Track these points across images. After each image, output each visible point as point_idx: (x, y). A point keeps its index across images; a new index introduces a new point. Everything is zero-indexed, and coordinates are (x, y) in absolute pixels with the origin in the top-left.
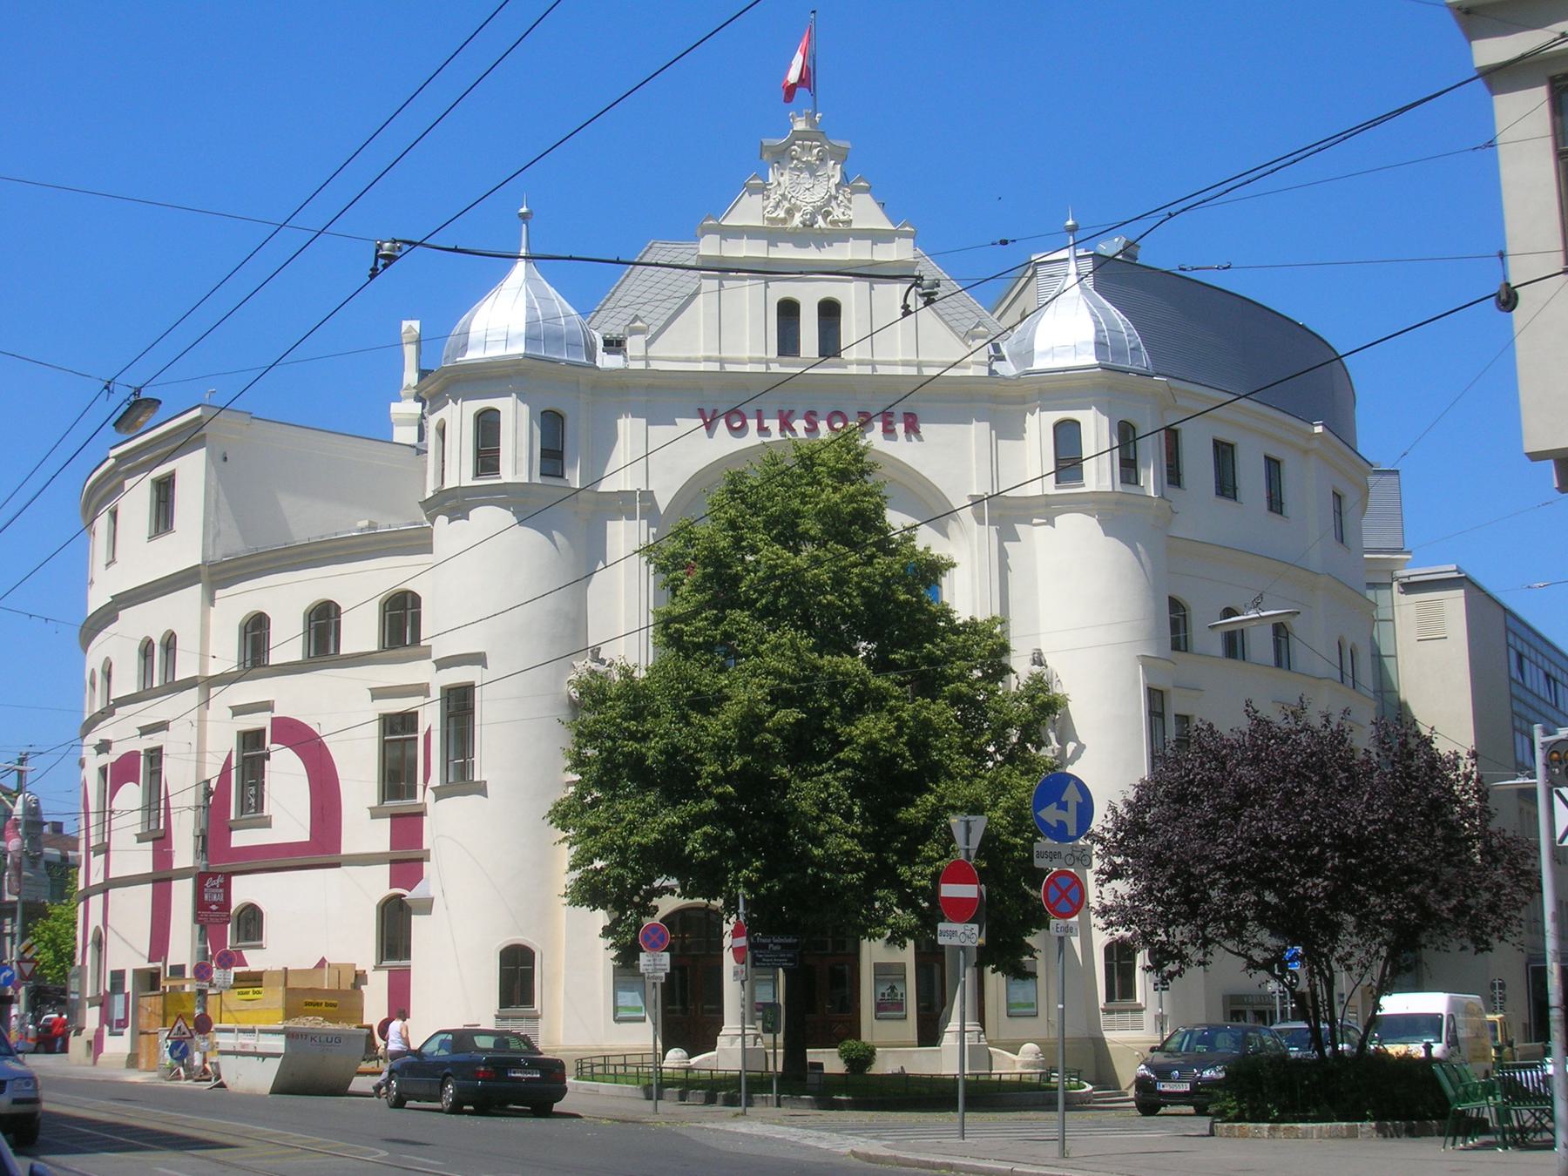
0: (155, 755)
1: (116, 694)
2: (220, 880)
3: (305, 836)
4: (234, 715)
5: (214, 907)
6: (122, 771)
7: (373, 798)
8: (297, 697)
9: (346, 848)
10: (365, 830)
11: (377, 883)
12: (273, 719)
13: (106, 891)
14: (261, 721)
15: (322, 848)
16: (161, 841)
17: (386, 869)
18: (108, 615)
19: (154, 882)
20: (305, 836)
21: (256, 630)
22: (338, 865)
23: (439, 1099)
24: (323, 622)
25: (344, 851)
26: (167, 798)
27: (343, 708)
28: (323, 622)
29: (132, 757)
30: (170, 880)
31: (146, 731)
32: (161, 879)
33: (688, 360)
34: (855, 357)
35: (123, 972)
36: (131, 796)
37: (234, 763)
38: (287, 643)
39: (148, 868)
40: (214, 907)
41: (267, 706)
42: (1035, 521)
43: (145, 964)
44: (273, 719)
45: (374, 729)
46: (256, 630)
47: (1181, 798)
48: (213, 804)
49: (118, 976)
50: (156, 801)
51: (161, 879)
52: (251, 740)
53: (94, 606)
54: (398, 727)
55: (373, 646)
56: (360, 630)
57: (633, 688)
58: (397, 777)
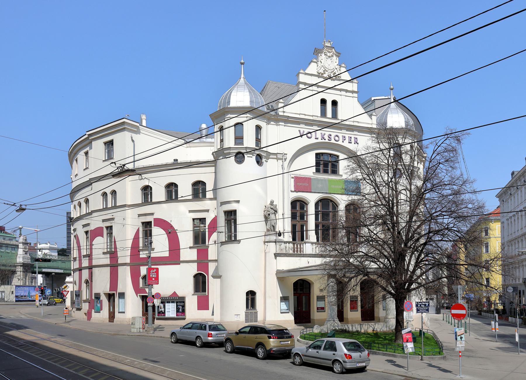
0: (110, 228)
1: (92, 208)
3: (167, 254)
4: (139, 217)
6: (98, 232)
7: (191, 244)
10: (188, 252)
11: (193, 269)
15: (174, 257)
16: (113, 254)
17: (195, 265)
20: (167, 254)
21: (147, 190)
22: (179, 264)
23: (114, 294)
24: (172, 190)
25: (181, 260)
27: (181, 216)
32: (114, 266)
33: (312, 116)
34: (342, 115)
36: (100, 243)
37: (141, 235)
39: (109, 263)
41: (152, 214)
42: (272, 123)
43: (108, 291)
46: (147, 190)
47: (376, 216)
48: (135, 249)
49: (98, 297)
50: (112, 241)
51: (114, 266)
52: (147, 225)
56: (185, 190)
58: (199, 239)
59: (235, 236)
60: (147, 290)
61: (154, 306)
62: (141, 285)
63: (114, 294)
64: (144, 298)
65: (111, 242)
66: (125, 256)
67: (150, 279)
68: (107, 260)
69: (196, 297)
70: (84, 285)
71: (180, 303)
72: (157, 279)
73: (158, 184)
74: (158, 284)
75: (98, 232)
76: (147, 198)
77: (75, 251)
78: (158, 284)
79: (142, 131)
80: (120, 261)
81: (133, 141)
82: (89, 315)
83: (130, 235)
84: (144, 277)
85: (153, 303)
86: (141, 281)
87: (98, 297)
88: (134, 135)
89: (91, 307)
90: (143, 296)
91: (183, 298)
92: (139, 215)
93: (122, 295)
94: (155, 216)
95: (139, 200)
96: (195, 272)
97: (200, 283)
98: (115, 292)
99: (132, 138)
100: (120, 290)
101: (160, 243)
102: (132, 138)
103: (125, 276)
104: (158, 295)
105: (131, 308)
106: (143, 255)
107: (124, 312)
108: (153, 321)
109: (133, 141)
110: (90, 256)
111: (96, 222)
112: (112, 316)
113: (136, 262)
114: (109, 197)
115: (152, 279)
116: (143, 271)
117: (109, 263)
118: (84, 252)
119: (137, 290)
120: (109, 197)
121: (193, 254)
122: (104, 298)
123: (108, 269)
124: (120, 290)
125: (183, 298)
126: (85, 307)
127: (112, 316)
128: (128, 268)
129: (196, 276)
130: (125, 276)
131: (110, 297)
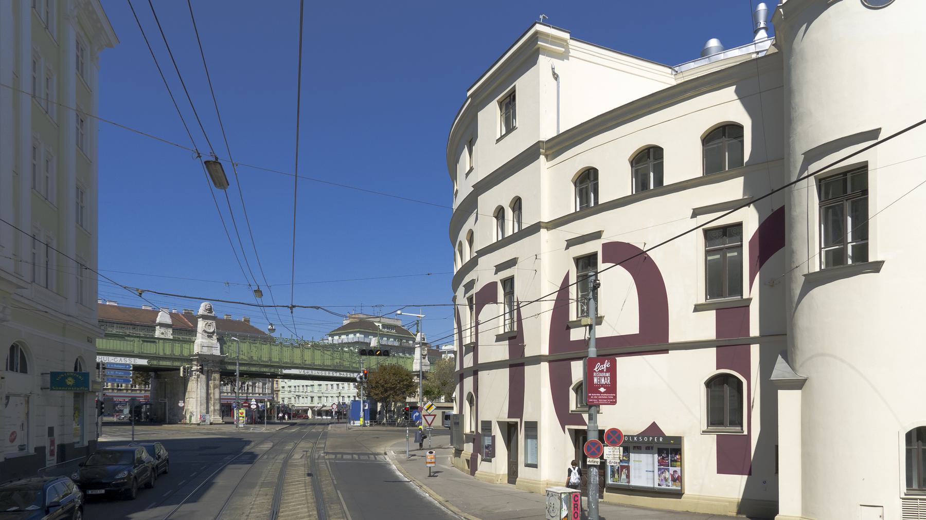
0: (509, 283)
2: (607, 364)
5: (602, 390)
6: (487, 295)
8: (617, 226)
9: (672, 339)
10: (691, 319)
11: (707, 363)
12: (604, 245)
13: (475, 373)
14: (594, 247)
15: (653, 336)
16: (514, 338)
17: (712, 352)
18: (471, 204)
19: (511, 366)
21: (587, 180)
22: (665, 351)
23: (517, 423)
24: (648, 161)
25: (671, 340)
26: (519, 308)
28: (648, 161)
29: (492, 286)
30: (523, 365)
31: (499, 268)
32: (517, 364)
35: (490, 422)
36: (495, 317)
37: (573, 292)
38: (616, 181)
39: (506, 356)
40: (602, 390)
41: (597, 235)
43: (505, 417)
44: (604, 245)
45: (697, 240)
46: (587, 180)
48: (560, 324)
49: (487, 426)
51: (517, 364)
52: (587, 263)
53: (456, 204)
54: (721, 238)
55: (699, 173)
57: (272, 401)
58: (721, 282)
59: (862, 252)
60: (586, 417)
61: (602, 466)
62: (573, 406)
63: (517, 423)
64: (579, 438)
65: (511, 312)
66: (538, 340)
67: (594, 389)
68: (502, 352)
69: (712, 440)
70: (466, 405)
71: (669, 450)
72: (612, 388)
73: (612, 158)
74: (614, 403)
75: (487, 295)
76: (588, 201)
77: (575, 297)
78: (614, 403)
79: (572, 53)
80: (528, 353)
81: (556, 76)
82: (472, 465)
83: (549, 286)
84: (578, 388)
85: (602, 457)
86: (573, 396)
87: (487, 426)
88: (557, 63)
89: (477, 450)
90: (576, 431)
91: (678, 440)
92: (571, 243)
93: (532, 428)
94: (606, 238)
95: (571, 205)
96: (712, 370)
97: (723, 397)
98: (518, 420)
99: (553, 69)
100: (528, 416)
101: (618, 304)
102: (553, 69)
103: (539, 380)
104: (613, 437)
105: (552, 459)
106: (577, 334)
107: (535, 466)
108: (601, 492)
109: (556, 76)
110: (473, 348)
111: (485, 274)
112: (513, 474)
113: (562, 351)
114: (509, 214)
115: (600, 392)
116: (577, 370)
117: (506, 356)
118: (467, 341)
119: (564, 416)
120: (509, 214)
121: (706, 326)
122: (497, 431)
123: (505, 373)
124: (528, 416)
125: (678, 440)
126: (468, 448)
127: (513, 474)
128: (545, 366)
129: (713, 383)
130: (539, 380)
131: (510, 431)
